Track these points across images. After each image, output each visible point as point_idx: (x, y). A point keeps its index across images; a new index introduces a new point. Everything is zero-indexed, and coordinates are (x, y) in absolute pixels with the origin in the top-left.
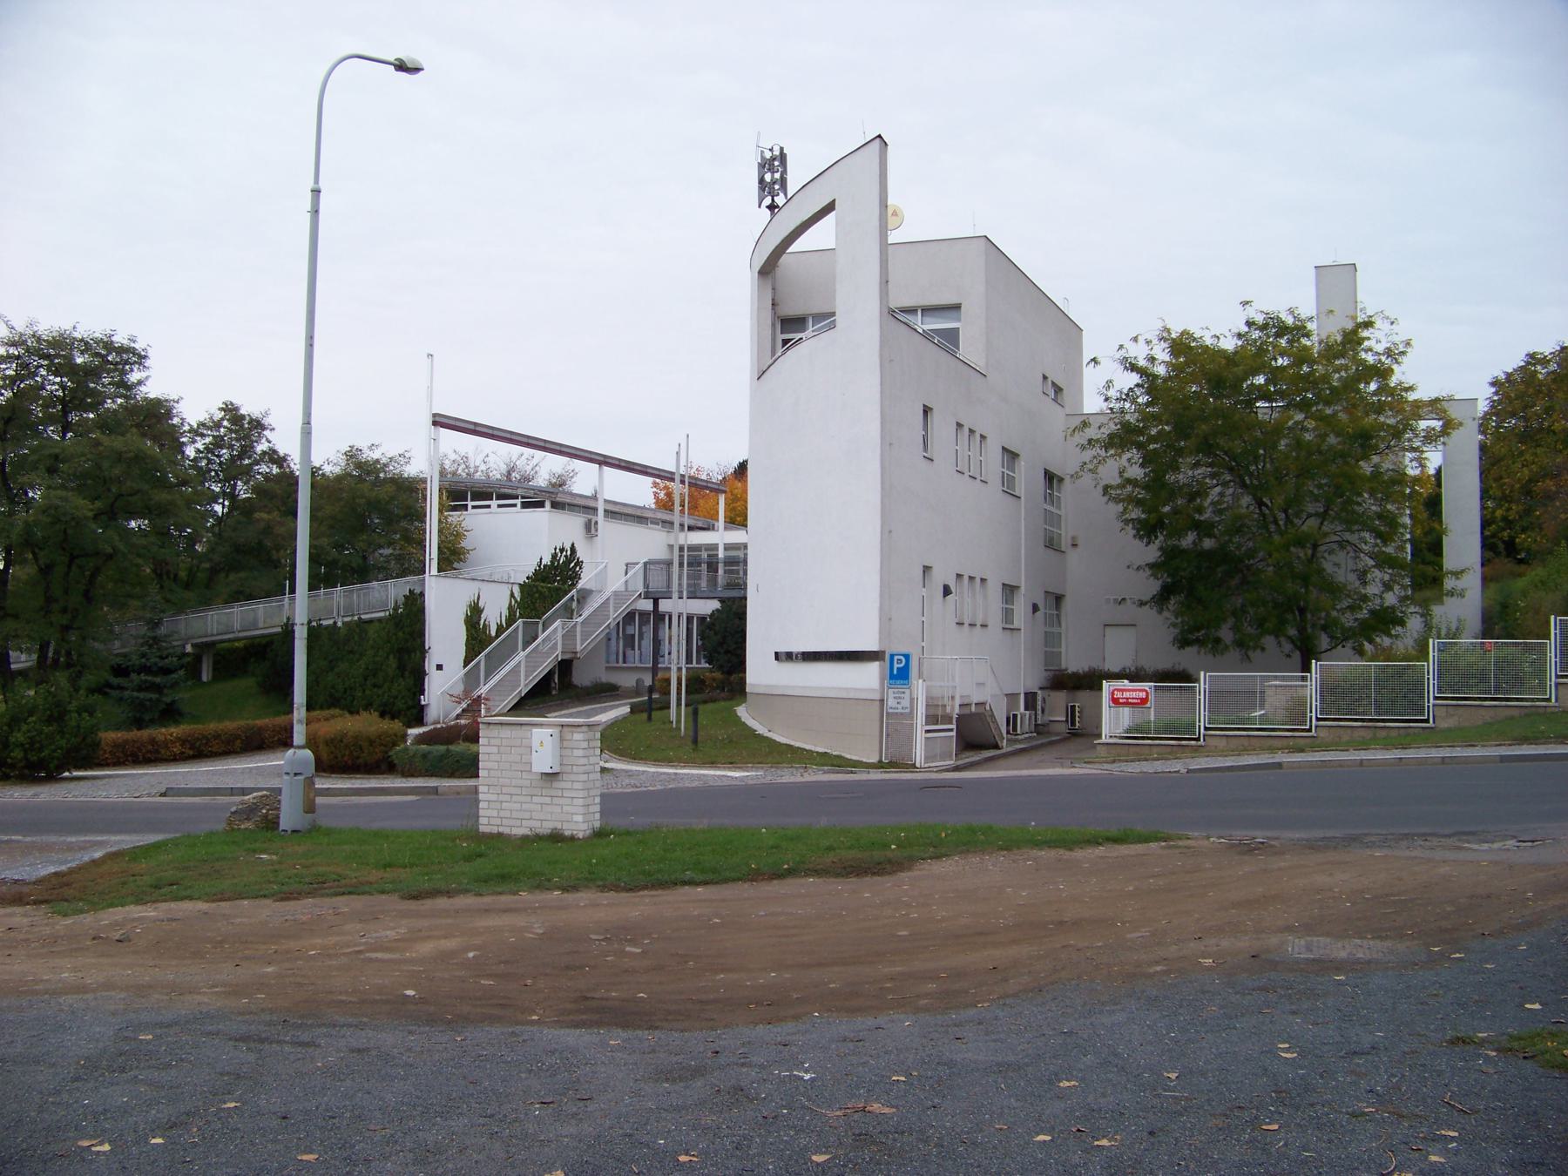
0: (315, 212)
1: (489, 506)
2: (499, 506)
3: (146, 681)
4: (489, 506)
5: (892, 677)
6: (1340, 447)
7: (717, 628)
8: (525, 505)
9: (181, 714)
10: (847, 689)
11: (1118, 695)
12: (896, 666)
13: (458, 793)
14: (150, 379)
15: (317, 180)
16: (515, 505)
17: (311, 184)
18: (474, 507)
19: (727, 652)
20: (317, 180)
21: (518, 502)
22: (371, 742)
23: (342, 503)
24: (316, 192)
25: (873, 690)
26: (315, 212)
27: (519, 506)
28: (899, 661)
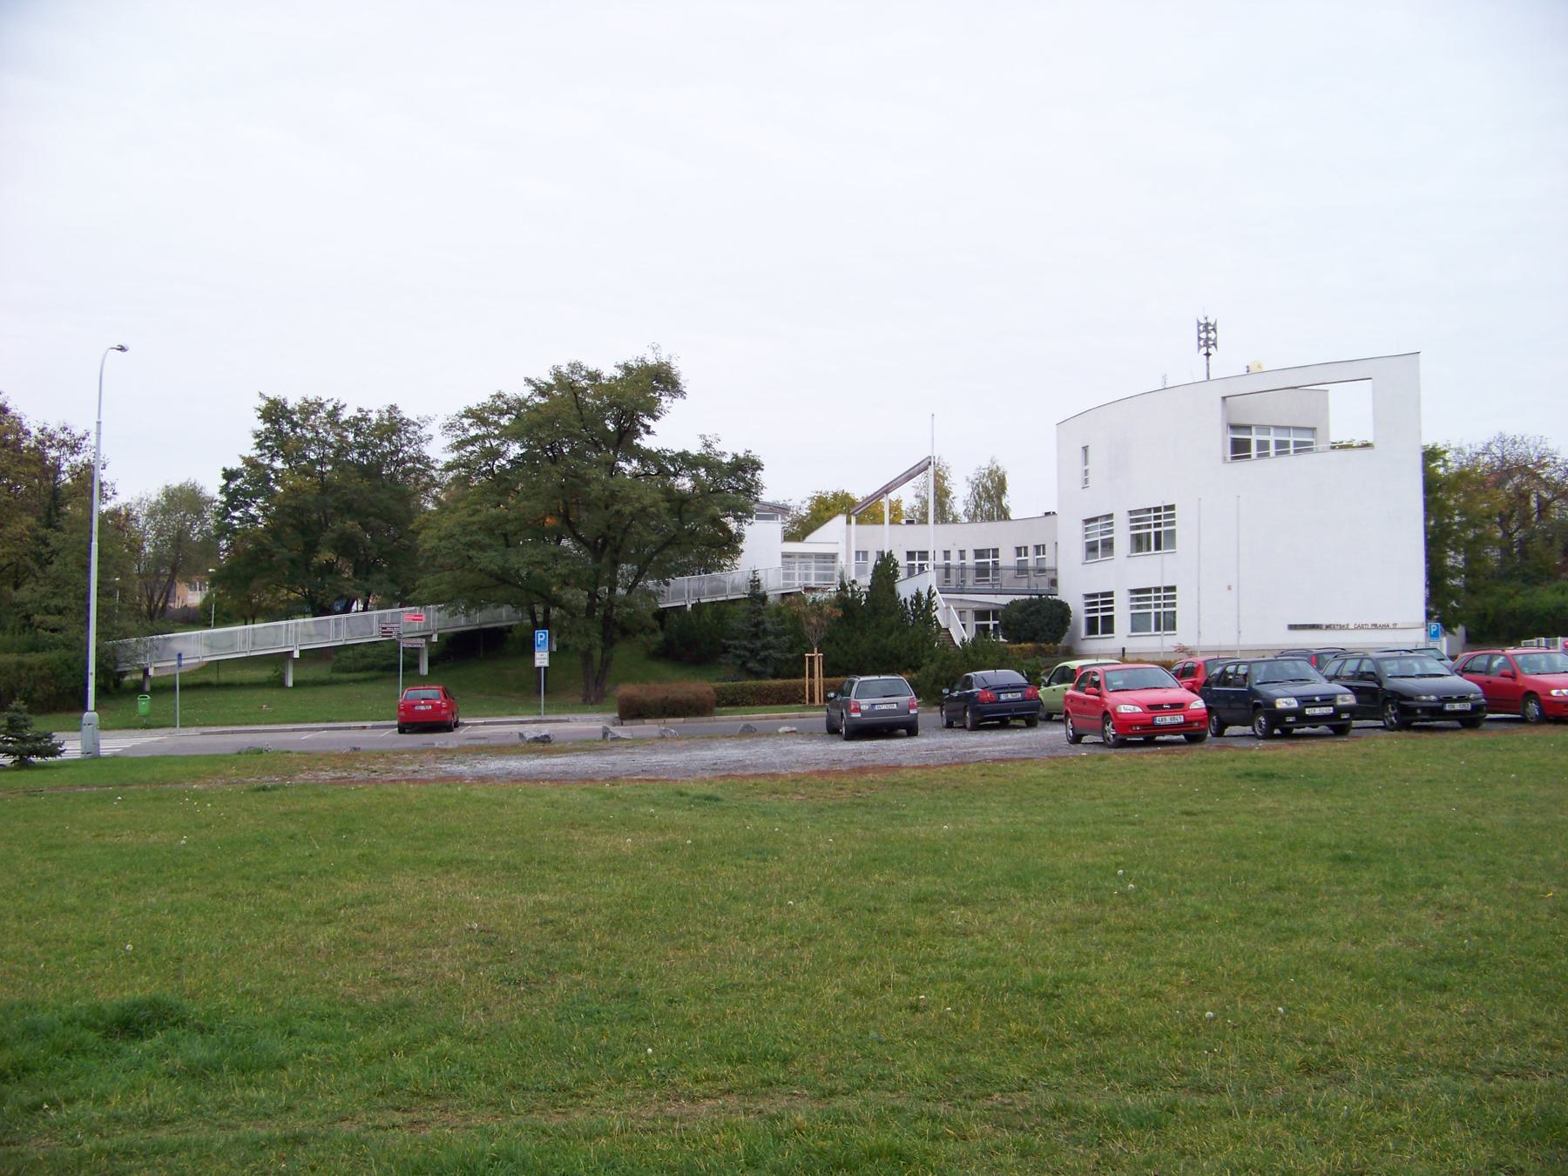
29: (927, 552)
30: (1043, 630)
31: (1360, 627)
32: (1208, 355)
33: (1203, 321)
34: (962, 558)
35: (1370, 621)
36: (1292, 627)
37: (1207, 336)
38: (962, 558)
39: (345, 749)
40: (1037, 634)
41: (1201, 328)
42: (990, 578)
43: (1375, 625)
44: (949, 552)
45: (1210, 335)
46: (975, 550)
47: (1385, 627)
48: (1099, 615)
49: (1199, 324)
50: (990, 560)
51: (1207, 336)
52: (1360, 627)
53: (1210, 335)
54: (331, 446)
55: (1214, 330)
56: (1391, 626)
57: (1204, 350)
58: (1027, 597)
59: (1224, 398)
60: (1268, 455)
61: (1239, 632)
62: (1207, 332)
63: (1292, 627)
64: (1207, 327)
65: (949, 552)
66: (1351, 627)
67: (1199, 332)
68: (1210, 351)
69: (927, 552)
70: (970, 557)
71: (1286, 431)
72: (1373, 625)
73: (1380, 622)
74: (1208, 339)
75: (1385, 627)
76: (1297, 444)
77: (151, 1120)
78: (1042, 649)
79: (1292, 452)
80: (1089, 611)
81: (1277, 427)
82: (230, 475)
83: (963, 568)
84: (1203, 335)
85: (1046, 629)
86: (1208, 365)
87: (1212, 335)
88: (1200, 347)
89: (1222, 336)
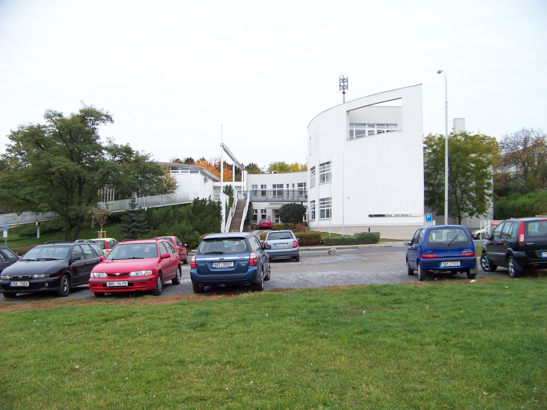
0: (446, 107)
1: (178, 172)
2: (182, 172)
3: (136, 225)
4: (178, 172)
5: (427, 220)
6: (107, 157)
7: (290, 210)
8: (191, 172)
9: (221, 232)
10: (413, 223)
11: (493, 223)
12: (428, 217)
13: (365, 248)
14: (109, 123)
15: (446, 100)
16: (188, 172)
17: (445, 101)
18: (172, 172)
19: (294, 217)
20: (446, 100)
21: (189, 171)
22: (315, 237)
23: (73, 166)
24: (446, 102)
25: (421, 223)
26: (446, 107)
27: (189, 172)
28: (429, 216)
29: (282, 185)
30: (291, 217)
31: (397, 216)
32: (344, 93)
33: (342, 78)
34: (294, 187)
35: (401, 213)
36: (370, 216)
37: (344, 84)
38: (294, 187)
39: (83, 264)
40: (288, 219)
41: (341, 81)
42: (303, 195)
43: (403, 215)
44: (288, 184)
45: (345, 84)
46: (298, 184)
47: (406, 216)
48: (325, 209)
49: (340, 79)
50: (303, 188)
51: (344, 84)
52: (397, 216)
53: (345, 84)
54: (486, 140)
55: (347, 81)
56: (409, 215)
57: (342, 91)
58: (293, 203)
59: (348, 112)
60: (353, 138)
61: (344, 219)
62: (343, 82)
63: (370, 216)
64: (344, 80)
65: (288, 184)
66: (393, 216)
67: (340, 83)
68: (345, 91)
69: (282, 185)
70: (296, 185)
71: (383, 126)
72: (402, 215)
73: (404, 213)
74: (344, 86)
75: (406, 216)
76: (369, 131)
77: (481, 288)
78: (288, 226)
79: (354, 138)
80: (321, 207)
81: (378, 125)
82: (203, 160)
83: (294, 191)
84: (342, 84)
85: (292, 217)
86: (344, 97)
87: (346, 84)
88: (340, 90)
89: (350, 83)
